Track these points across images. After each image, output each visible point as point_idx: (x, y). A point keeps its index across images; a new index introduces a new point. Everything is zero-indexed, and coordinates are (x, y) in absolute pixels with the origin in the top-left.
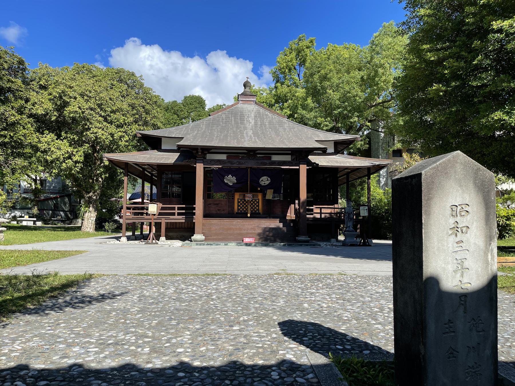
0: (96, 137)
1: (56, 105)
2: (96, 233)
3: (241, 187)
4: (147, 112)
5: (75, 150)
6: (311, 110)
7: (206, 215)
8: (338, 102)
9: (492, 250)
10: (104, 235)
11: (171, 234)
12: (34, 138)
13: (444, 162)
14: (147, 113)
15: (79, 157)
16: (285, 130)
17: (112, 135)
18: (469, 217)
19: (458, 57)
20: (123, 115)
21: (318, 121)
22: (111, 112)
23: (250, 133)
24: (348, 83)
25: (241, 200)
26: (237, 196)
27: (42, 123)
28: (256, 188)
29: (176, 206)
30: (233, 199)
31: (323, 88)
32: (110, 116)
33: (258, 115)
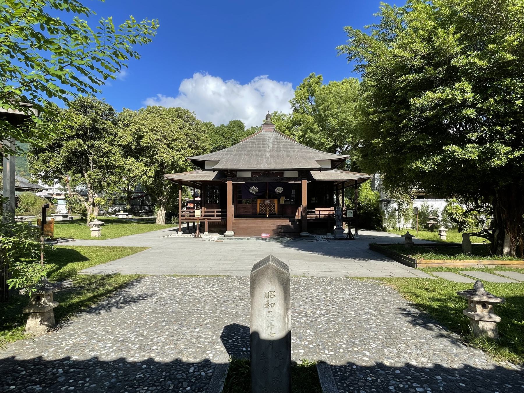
0: (162, 159)
1: (134, 137)
2: (166, 225)
3: (261, 195)
4: (198, 139)
5: (148, 169)
6: (318, 133)
7: (237, 216)
8: (336, 127)
9: (288, 316)
10: (170, 227)
11: (213, 229)
12: (121, 161)
13: (262, 268)
14: (198, 140)
15: (151, 173)
16: (294, 151)
17: (173, 157)
18: (275, 298)
19: (390, 119)
20: (181, 142)
21: (322, 141)
22: (172, 141)
23: (268, 155)
24: (345, 112)
25: (262, 204)
26: (259, 202)
27: (127, 151)
28: (273, 196)
29: (215, 210)
30: (256, 204)
31: (326, 116)
32: (171, 144)
33: (276, 140)
